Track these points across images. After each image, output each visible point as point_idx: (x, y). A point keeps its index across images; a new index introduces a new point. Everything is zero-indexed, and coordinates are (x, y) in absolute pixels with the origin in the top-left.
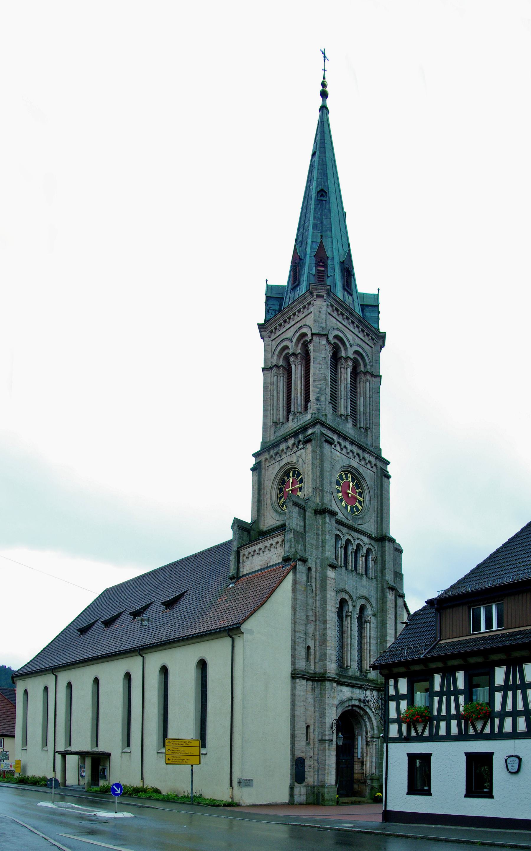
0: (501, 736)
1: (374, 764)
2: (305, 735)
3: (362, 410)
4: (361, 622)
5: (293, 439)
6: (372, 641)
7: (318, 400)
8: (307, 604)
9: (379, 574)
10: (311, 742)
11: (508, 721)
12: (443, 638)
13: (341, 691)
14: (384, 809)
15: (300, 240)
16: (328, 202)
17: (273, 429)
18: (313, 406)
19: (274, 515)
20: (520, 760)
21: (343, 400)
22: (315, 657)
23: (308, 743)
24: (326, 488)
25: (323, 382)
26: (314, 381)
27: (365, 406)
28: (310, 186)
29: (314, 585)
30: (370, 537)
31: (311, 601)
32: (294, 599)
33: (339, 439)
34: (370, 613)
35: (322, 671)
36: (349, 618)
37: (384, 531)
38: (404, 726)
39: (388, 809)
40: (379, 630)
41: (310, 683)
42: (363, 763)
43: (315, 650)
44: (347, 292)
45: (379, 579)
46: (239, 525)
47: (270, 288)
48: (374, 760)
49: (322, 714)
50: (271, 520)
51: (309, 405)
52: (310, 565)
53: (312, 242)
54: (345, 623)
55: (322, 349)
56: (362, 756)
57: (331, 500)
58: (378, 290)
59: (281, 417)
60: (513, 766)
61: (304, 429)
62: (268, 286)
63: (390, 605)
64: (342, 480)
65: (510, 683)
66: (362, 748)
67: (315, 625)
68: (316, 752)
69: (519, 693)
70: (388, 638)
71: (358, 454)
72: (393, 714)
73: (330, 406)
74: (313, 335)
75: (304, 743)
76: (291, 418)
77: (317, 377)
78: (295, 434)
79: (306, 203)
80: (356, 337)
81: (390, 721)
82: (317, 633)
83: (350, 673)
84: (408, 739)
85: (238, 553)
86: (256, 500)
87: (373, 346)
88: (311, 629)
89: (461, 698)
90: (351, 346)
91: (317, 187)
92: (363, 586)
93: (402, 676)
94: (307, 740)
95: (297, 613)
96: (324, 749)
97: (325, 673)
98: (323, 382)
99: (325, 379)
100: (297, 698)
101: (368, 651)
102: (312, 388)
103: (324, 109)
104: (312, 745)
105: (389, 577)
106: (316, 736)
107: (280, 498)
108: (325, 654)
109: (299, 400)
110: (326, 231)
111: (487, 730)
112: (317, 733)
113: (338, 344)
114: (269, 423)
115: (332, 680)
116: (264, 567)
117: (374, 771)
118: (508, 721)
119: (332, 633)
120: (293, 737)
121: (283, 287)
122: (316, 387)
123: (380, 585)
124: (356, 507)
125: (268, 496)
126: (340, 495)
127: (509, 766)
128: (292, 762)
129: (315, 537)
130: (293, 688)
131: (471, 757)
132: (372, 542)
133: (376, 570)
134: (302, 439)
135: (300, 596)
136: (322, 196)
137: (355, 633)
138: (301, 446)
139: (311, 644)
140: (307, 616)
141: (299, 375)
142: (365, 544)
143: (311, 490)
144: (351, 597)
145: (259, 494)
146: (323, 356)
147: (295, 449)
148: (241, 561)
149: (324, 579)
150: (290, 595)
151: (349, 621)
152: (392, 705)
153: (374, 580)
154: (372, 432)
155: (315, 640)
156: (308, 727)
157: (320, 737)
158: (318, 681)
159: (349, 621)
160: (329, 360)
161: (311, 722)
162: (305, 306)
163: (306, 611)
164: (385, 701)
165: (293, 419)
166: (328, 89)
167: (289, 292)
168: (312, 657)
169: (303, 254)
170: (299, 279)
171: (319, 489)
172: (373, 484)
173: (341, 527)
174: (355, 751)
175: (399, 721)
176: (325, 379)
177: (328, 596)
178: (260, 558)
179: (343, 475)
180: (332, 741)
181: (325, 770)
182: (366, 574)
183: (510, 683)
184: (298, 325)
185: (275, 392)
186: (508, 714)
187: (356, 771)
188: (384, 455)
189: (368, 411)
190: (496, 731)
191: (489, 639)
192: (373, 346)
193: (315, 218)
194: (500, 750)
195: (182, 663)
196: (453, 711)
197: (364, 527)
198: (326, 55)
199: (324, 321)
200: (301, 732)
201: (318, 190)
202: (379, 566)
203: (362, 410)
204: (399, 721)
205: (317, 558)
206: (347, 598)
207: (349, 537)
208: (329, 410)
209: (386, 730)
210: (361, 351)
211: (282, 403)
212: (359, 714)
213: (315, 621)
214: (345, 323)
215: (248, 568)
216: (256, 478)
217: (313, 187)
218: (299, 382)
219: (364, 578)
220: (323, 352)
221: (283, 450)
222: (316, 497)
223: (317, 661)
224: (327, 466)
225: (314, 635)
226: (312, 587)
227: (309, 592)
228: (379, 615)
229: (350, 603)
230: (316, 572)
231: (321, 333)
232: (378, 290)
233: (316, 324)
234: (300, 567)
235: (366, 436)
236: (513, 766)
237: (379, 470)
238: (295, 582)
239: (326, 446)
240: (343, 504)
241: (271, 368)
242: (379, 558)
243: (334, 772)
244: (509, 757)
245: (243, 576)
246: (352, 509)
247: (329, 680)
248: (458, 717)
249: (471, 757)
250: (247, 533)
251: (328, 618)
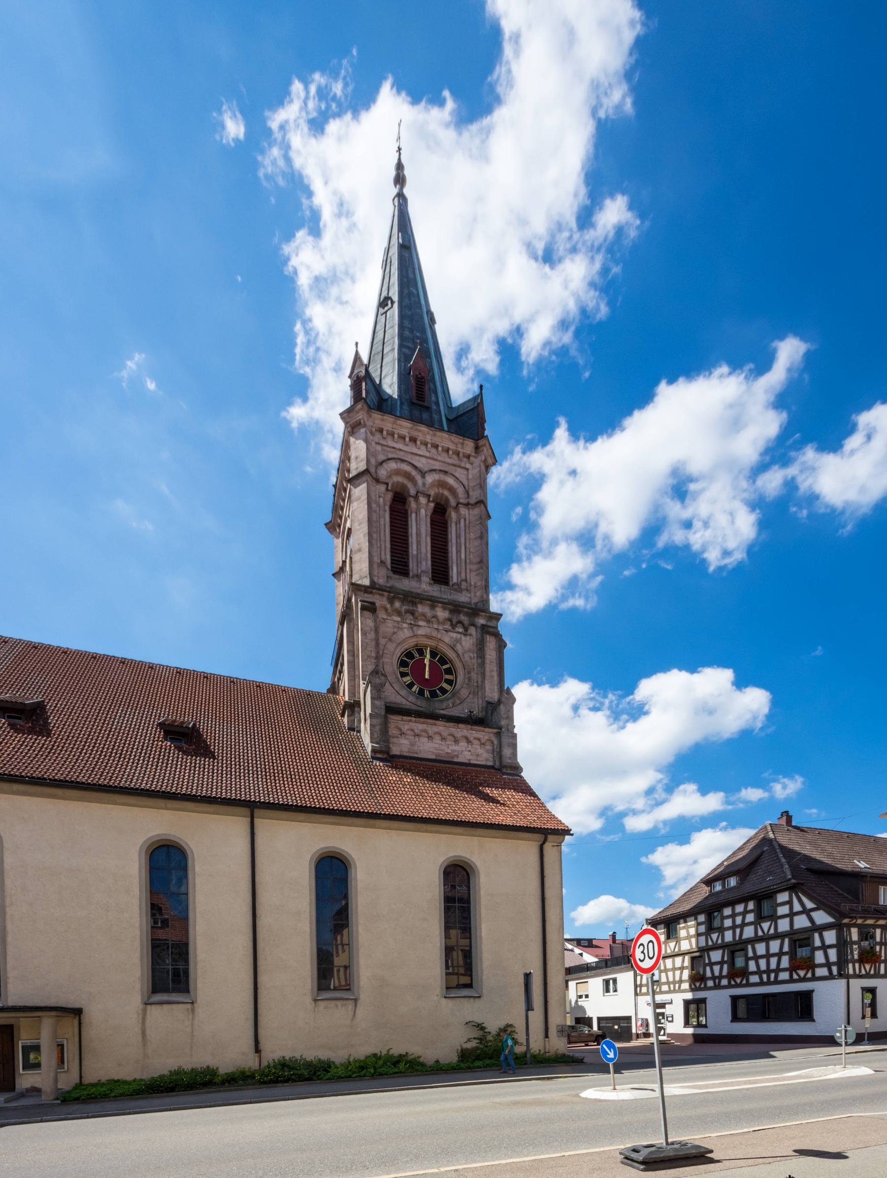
84: (860, 976)
103: (401, 196)
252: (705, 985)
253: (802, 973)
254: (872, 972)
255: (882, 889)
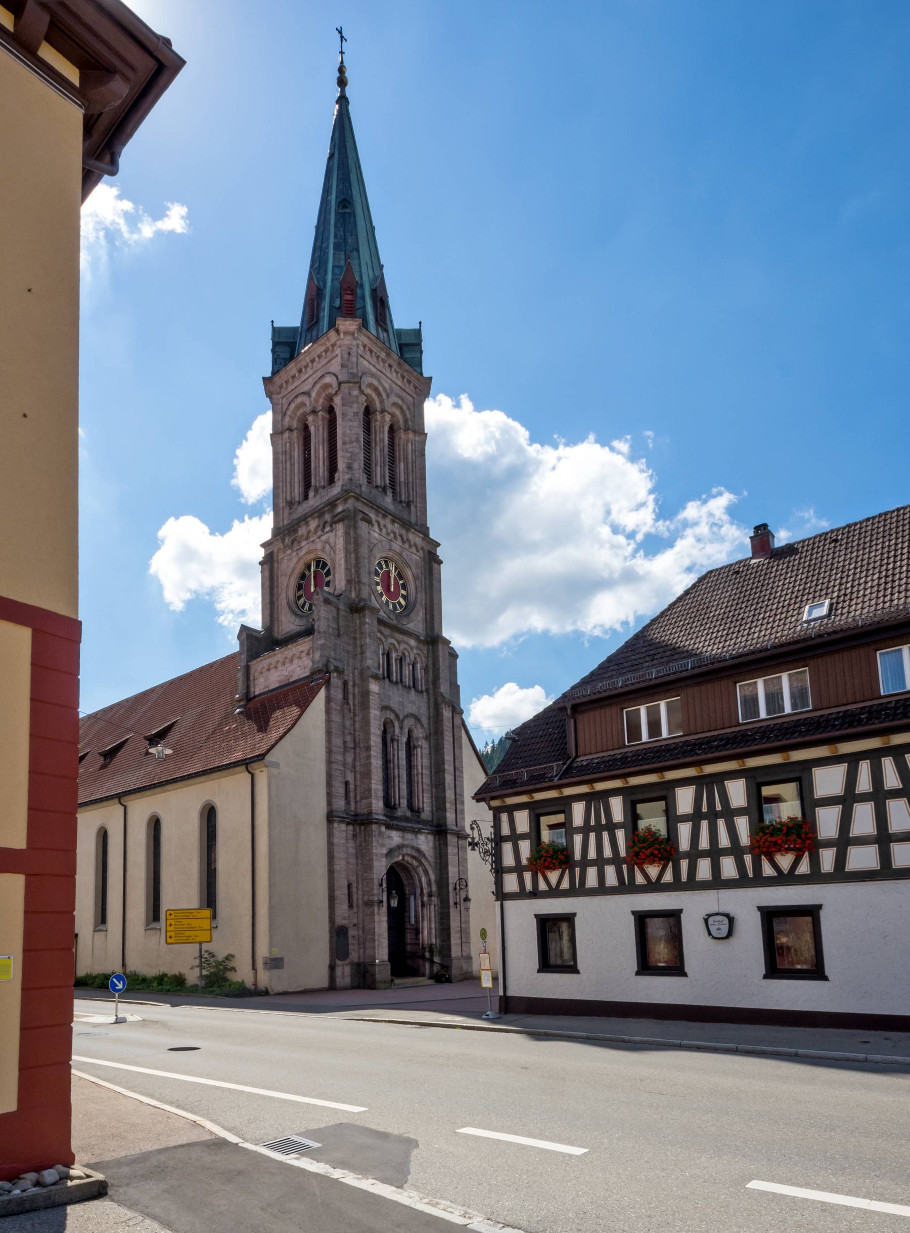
0: (693, 884)
1: (433, 931)
2: (347, 896)
3: (402, 479)
4: (410, 748)
5: (317, 520)
6: (424, 772)
7: (349, 467)
8: (344, 727)
9: (431, 686)
10: (355, 905)
11: (592, 872)
12: (581, 751)
13: (389, 837)
14: (501, 993)
15: (317, 265)
16: (353, 215)
17: (287, 511)
18: (342, 476)
19: (292, 618)
20: (731, 920)
21: (379, 468)
22: (356, 794)
23: (351, 906)
24: (365, 579)
25: (355, 444)
26: (344, 443)
27: (407, 474)
28: (327, 196)
29: (351, 703)
30: (417, 639)
31: (348, 723)
32: (328, 721)
33: (377, 516)
34: (421, 735)
35: (365, 811)
36: (395, 743)
37: (436, 631)
38: (528, 876)
39: (511, 993)
40: (433, 756)
41: (351, 827)
42: (417, 931)
43: (356, 786)
44: (381, 326)
45: (431, 692)
46: (246, 632)
47: (277, 332)
48: (433, 926)
49: (368, 867)
50: (288, 624)
51: (336, 475)
52: (346, 678)
53: (334, 267)
54: (390, 750)
55: (353, 402)
56: (417, 921)
57: (370, 594)
58: (420, 323)
59: (297, 495)
60: (719, 929)
61: (332, 504)
62: (274, 329)
63: (447, 725)
64: (381, 568)
65: (593, 823)
66: (416, 911)
67: (355, 753)
68: (361, 919)
69: (605, 835)
70: (446, 767)
71: (401, 536)
72: (508, 860)
73: (365, 476)
74: (340, 384)
75: (345, 906)
76: (311, 494)
77: (347, 439)
78: (319, 513)
79: (322, 218)
80: (394, 386)
81: (893, 838)
82: (358, 764)
83: (399, 813)
84: (535, 894)
85: (247, 668)
86: (268, 601)
87: (415, 396)
88: (349, 758)
89: (620, 834)
90: (388, 396)
91: (337, 197)
92: (413, 703)
93: (520, 807)
94: (349, 902)
95: (333, 739)
96: (373, 914)
97: (370, 813)
98: (355, 444)
99: (357, 440)
100: (336, 848)
101: (420, 785)
102: (340, 454)
103: (343, 100)
104: (355, 910)
105: (444, 688)
106: (360, 897)
107: (300, 597)
108: (370, 790)
109: (321, 471)
110: (352, 251)
111: (804, 868)
112: (360, 892)
113: (371, 396)
114: (282, 504)
115: (378, 822)
116: (283, 683)
117: (434, 941)
118: (592, 872)
119: (376, 763)
120: (332, 899)
121: (294, 329)
122: (347, 452)
123: (432, 700)
124: (399, 603)
125: (283, 596)
126: (379, 588)
127: (713, 929)
128: (331, 932)
129: (352, 642)
130: (330, 835)
131: (642, 919)
132: (422, 646)
133: (427, 682)
134: (329, 520)
135: (336, 717)
136: (345, 207)
137: (403, 762)
138: (328, 529)
139: (350, 777)
140: (345, 742)
141: (321, 438)
142: (412, 648)
143: (343, 583)
144: (397, 716)
145: (272, 594)
146: (355, 410)
147: (320, 533)
148: (252, 678)
149: (366, 694)
150: (323, 716)
151: (395, 747)
152: (507, 848)
153: (425, 693)
154: (416, 507)
155: (355, 772)
156: (349, 886)
157: (366, 898)
158: (361, 824)
159: (395, 747)
160: (361, 416)
161: (353, 879)
162: (328, 348)
163: (344, 735)
164: (496, 844)
165: (315, 496)
166: (348, 75)
167: (303, 334)
168: (352, 795)
169: (321, 283)
170: (318, 315)
171: (354, 581)
172: (419, 572)
173: (382, 628)
174: (406, 914)
175: (518, 869)
176: (357, 440)
177: (372, 716)
178: (278, 673)
179: (383, 563)
180: (382, 902)
181: (374, 941)
182: (414, 686)
183: (593, 823)
184: (319, 374)
185: (288, 464)
186: (593, 863)
187: (409, 941)
188: (432, 535)
189: (411, 479)
190: (684, 877)
191: (663, 751)
192: (415, 396)
193: (336, 236)
194: (694, 907)
195: (179, 810)
196: (608, 853)
197: (411, 626)
198: (344, 34)
199: (355, 366)
200: (341, 894)
201: (339, 200)
202: (431, 675)
203: (402, 479)
204: (518, 869)
205: (355, 668)
206: (392, 717)
207: (393, 641)
208: (362, 478)
209: (499, 883)
210: (400, 402)
211: (298, 477)
212: (412, 865)
213: (355, 748)
214: (380, 366)
215: (262, 687)
216: (267, 574)
217: (333, 197)
218: (321, 447)
219: (413, 692)
220: (355, 405)
221: (302, 536)
222: (350, 591)
223: (358, 799)
224: (364, 551)
225: (354, 766)
226: (351, 705)
227: (346, 711)
228: (432, 737)
229: (396, 724)
230: (354, 686)
231: (352, 380)
232: (420, 323)
233: (344, 370)
234: (335, 680)
235: (410, 512)
236: (719, 929)
237: (426, 555)
238: (328, 700)
239: (363, 526)
240: (384, 598)
241: (282, 433)
242: (431, 665)
243: (385, 943)
244: (710, 916)
245: (255, 697)
246: (394, 605)
247: (376, 823)
248: (616, 860)
249: (642, 919)
250: (256, 644)
251: (372, 743)
252: (815, 862)
253: (653, 871)
254: (565, 885)
255: (905, 649)
